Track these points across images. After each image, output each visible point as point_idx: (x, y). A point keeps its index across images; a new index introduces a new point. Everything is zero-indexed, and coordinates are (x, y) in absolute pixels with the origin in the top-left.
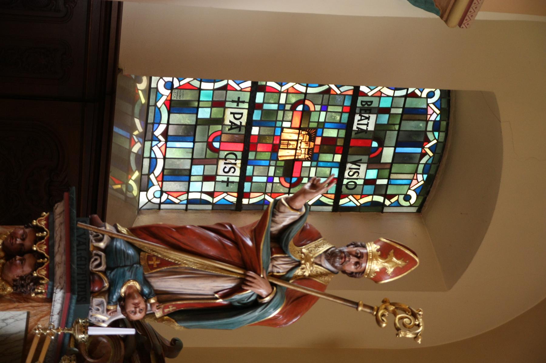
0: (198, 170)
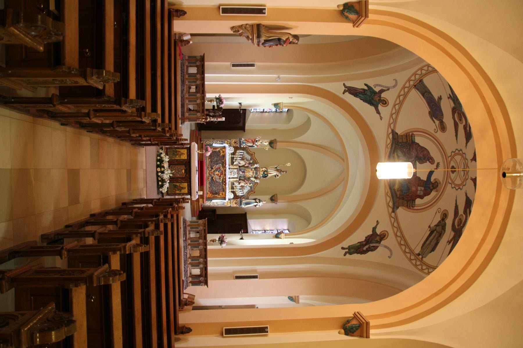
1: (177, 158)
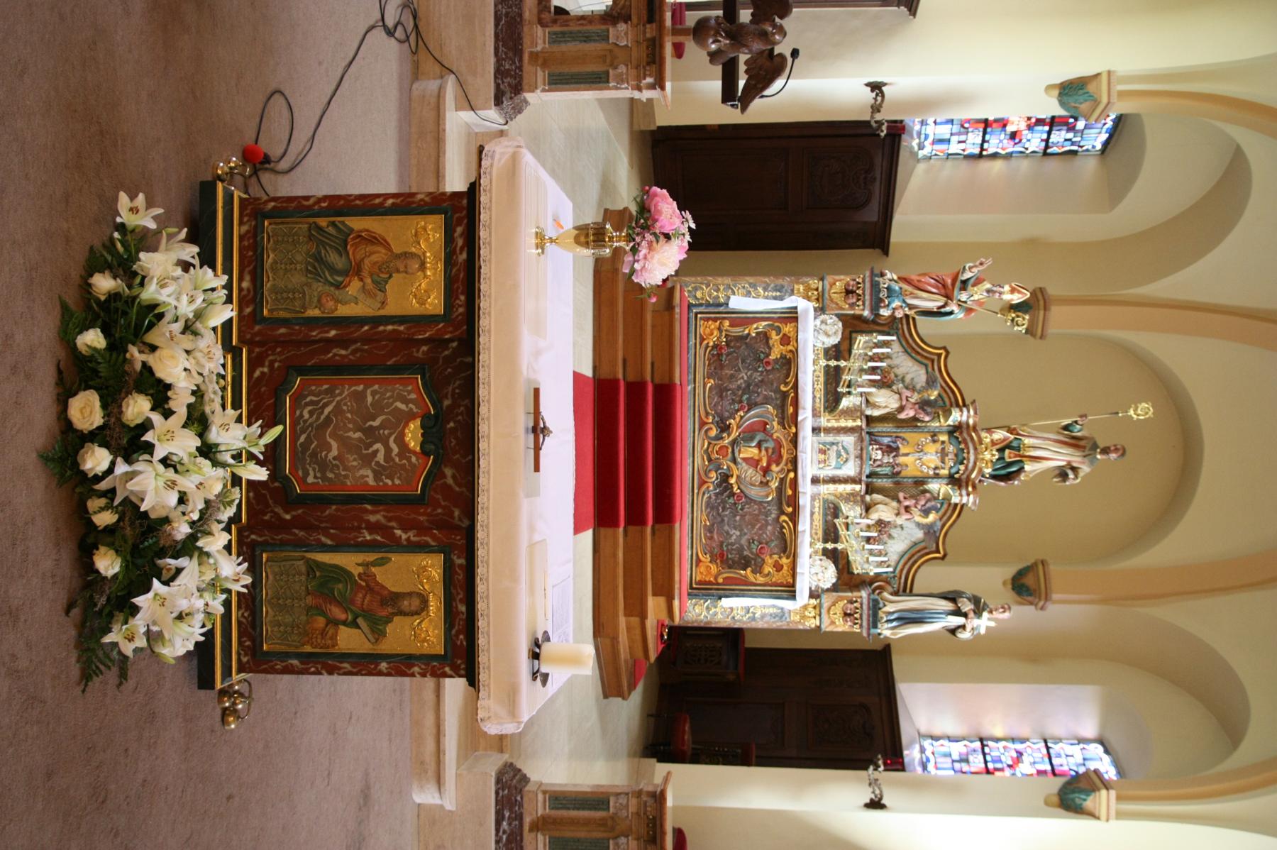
0: (955, 139)
1: (354, 302)
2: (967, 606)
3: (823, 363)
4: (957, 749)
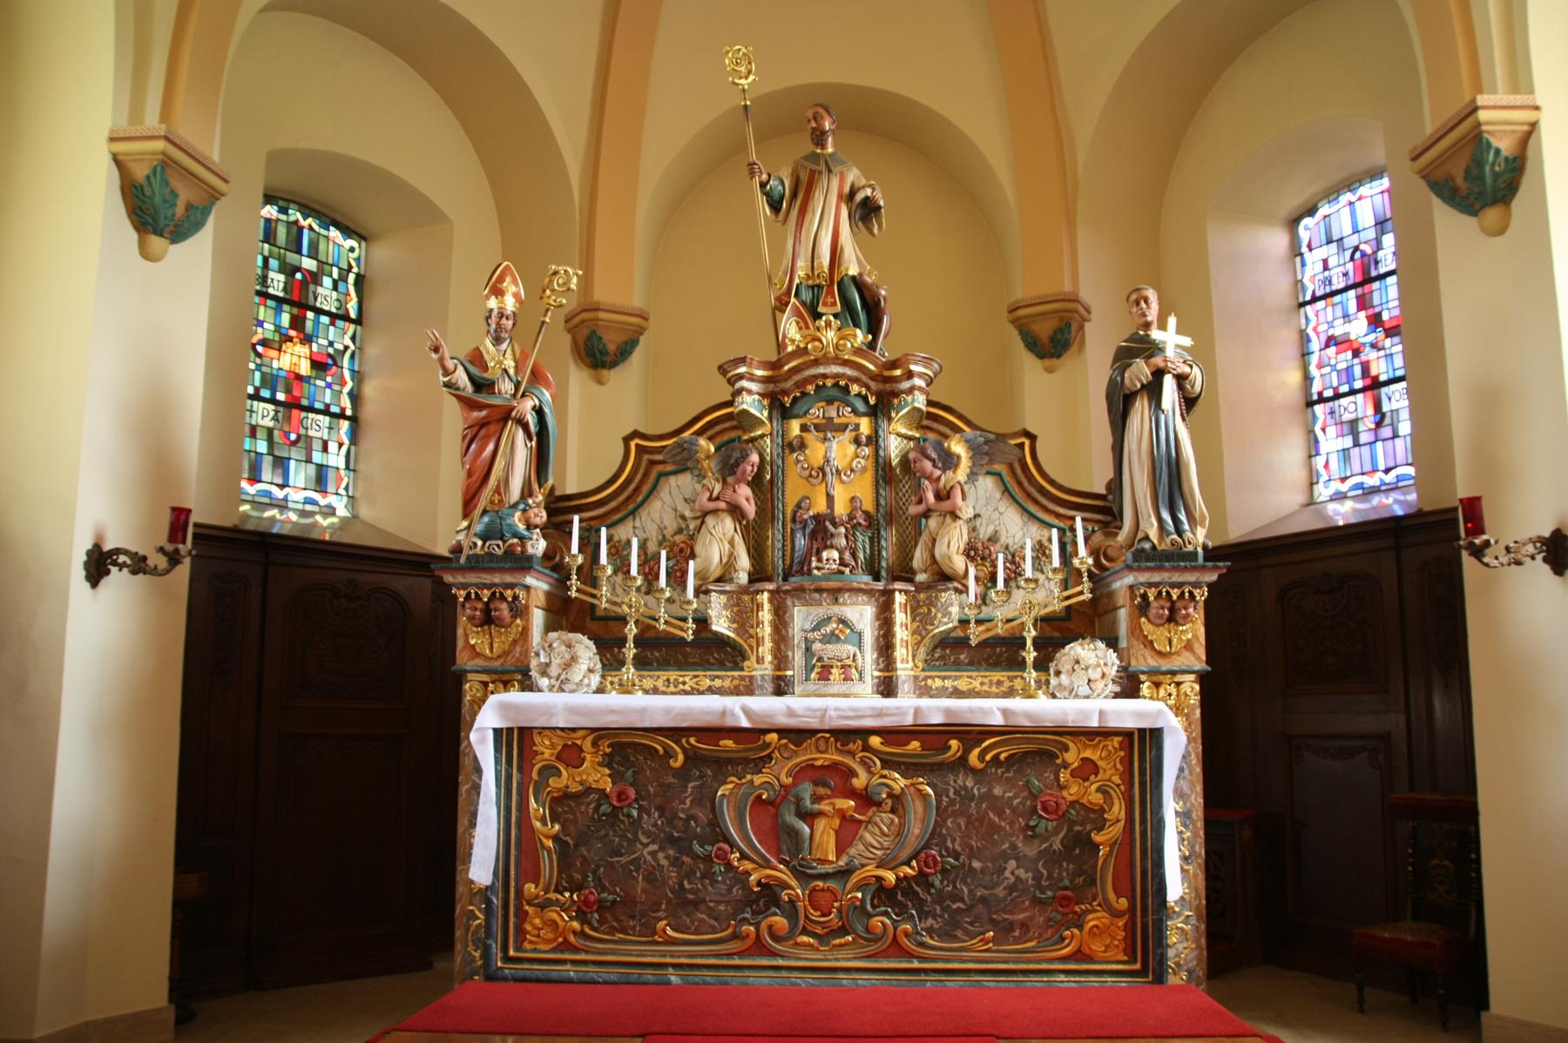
0: (317, 457)
2: (1140, 371)
3: (629, 672)
4: (1332, 442)
